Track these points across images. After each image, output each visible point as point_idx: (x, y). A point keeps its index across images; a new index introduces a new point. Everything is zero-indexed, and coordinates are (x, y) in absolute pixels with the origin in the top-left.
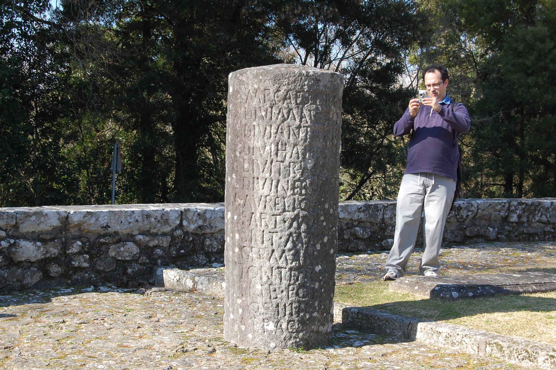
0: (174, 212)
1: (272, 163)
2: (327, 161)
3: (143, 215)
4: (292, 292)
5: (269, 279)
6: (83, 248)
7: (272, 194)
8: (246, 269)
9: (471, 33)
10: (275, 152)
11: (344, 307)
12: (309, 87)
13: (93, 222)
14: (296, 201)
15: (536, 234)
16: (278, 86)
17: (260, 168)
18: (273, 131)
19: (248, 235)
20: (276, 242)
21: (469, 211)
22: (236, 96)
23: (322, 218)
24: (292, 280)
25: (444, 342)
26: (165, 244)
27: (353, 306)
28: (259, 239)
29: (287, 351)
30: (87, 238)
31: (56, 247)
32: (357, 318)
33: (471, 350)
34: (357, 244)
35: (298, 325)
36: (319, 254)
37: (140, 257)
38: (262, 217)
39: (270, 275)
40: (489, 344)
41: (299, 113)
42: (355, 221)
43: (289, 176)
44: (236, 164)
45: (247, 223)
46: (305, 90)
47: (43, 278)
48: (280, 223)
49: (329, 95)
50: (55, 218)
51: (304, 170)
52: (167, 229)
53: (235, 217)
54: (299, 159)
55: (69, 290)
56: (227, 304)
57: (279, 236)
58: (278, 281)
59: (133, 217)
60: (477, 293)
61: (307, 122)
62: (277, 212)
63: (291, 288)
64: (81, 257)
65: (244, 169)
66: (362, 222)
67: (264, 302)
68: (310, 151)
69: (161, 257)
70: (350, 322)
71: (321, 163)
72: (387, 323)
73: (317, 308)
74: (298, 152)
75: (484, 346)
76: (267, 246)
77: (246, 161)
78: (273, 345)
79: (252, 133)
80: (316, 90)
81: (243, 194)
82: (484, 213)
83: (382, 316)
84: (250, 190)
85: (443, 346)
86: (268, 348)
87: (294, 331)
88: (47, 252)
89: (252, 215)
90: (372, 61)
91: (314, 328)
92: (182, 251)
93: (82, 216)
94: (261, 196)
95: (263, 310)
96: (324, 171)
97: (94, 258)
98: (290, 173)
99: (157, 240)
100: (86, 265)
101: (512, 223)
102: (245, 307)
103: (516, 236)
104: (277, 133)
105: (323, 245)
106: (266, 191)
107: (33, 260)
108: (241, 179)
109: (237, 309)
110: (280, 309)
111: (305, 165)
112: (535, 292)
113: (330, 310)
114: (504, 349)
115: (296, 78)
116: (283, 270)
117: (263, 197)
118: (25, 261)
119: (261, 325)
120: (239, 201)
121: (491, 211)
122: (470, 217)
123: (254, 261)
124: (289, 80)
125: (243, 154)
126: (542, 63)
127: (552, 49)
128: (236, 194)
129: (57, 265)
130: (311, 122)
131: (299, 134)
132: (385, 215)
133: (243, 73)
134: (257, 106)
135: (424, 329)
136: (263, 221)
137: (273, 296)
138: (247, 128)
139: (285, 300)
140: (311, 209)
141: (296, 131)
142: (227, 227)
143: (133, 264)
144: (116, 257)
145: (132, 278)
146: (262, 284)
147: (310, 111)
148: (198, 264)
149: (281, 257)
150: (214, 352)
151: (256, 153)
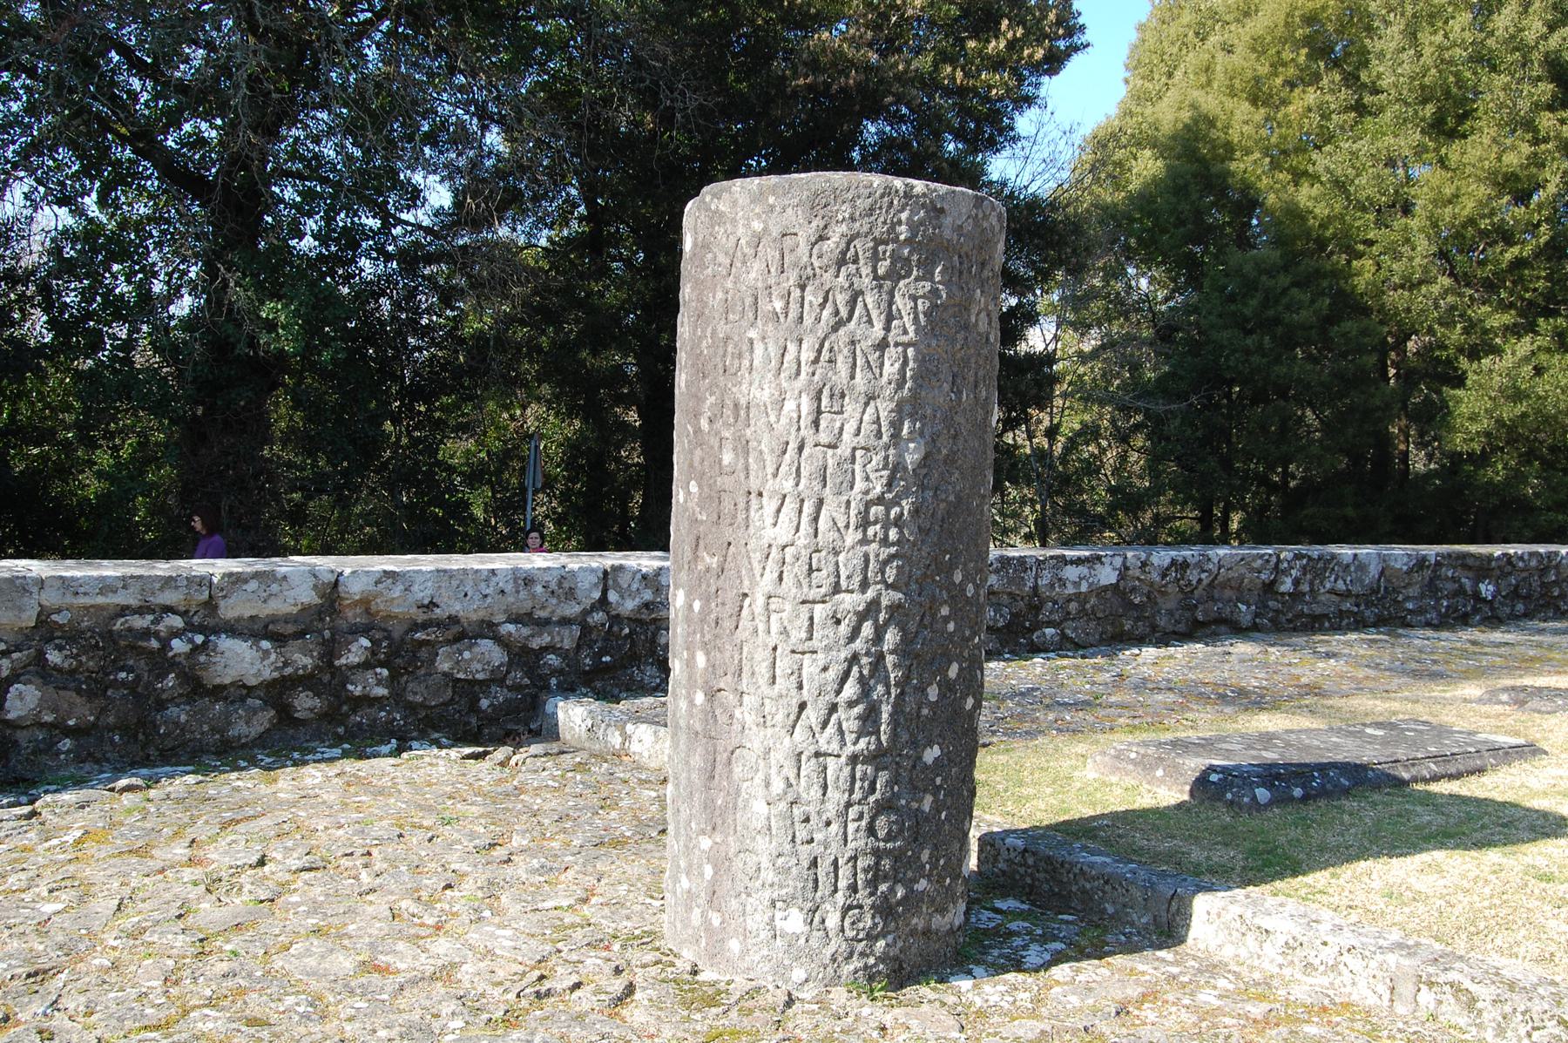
1: (801, 448)
3: (515, 580)
4: (856, 824)
5: (790, 785)
6: (374, 653)
7: (803, 539)
8: (725, 755)
9: (1148, 261)
10: (811, 418)
13: (397, 594)
14: (872, 561)
15: (1326, 616)
16: (822, 224)
17: (768, 463)
18: (807, 355)
19: (732, 657)
21: (1204, 571)
23: (945, 611)
25: (1280, 959)
26: (567, 644)
27: (1007, 827)
28: (764, 671)
29: (839, 995)
30: (385, 630)
31: (307, 652)
33: (1365, 990)
35: (873, 917)
36: (935, 713)
37: (508, 672)
38: (772, 607)
40: (1431, 984)
41: (884, 305)
43: (852, 488)
44: (698, 452)
45: (728, 624)
46: (902, 237)
47: (279, 723)
49: (967, 256)
50: (305, 586)
51: (895, 471)
52: (572, 610)
53: (697, 605)
54: (881, 438)
55: (337, 751)
57: (821, 664)
58: (815, 792)
59: (492, 584)
60: (1313, 788)
61: (905, 332)
62: (814, 594)
64: (369, 675)
67: (775, 853)
68: (913, 416)
70: (1004, 872)
71: (944, 452)
73: (928, 866)
74: (878, 418)
75: (1411, 988)
76: (784, 692)
77: (728, 446)
78: (798, 974)
79: (746, 363)
80: (931, 240)
81: (718, 538)
82: (1231, 574)
83: (1092, 865)
84: (739, 527)
85: (1278, 970)
87: (860, 936)
88: (286, 664)
89: (742, 601)
91: (918, 922)
92: (607, 659)
93: (372, 580)
94: (770, 546)
96: (951, 474)
97: (402, 675)
98: (854, 478)
100: (381, 691)
101: (1283, 594)
102: (721, 862)
103: (1290, 621)
104: (816, 361)
105: (947, 687)
106: (783, 533)
107: (253, 682)
108: (712, 497)
109: (700, 866)
111: (900, 456)
112: (1436, 778)
114: (1480, 1005)
116: (831, 762)
117: (774, 550)
118: (232, 684)
119: (766, 919)
120: (708, 559)
121: (1243, 570)
122: (1205, 582)
124: (854, 207)
125: (718, 425)
126: (1271, 313)
127: (1288, 288)
128: (698, 538)
129: (310, 694)
130: (916, 332)
131: (882, 365)
133: (722, 191)
134: (760, 284)
135: (1219, 915)
136: (774, 617)
137: (802, 835)
138: (730, 349)
139: (834, 848)
141: (873, 357)
142: (675, 630)
143: (493, 689)
145: (491, 719)
147: (914, 298)
149: (825, 724)
150: (628, 996)
151: (758, 423)
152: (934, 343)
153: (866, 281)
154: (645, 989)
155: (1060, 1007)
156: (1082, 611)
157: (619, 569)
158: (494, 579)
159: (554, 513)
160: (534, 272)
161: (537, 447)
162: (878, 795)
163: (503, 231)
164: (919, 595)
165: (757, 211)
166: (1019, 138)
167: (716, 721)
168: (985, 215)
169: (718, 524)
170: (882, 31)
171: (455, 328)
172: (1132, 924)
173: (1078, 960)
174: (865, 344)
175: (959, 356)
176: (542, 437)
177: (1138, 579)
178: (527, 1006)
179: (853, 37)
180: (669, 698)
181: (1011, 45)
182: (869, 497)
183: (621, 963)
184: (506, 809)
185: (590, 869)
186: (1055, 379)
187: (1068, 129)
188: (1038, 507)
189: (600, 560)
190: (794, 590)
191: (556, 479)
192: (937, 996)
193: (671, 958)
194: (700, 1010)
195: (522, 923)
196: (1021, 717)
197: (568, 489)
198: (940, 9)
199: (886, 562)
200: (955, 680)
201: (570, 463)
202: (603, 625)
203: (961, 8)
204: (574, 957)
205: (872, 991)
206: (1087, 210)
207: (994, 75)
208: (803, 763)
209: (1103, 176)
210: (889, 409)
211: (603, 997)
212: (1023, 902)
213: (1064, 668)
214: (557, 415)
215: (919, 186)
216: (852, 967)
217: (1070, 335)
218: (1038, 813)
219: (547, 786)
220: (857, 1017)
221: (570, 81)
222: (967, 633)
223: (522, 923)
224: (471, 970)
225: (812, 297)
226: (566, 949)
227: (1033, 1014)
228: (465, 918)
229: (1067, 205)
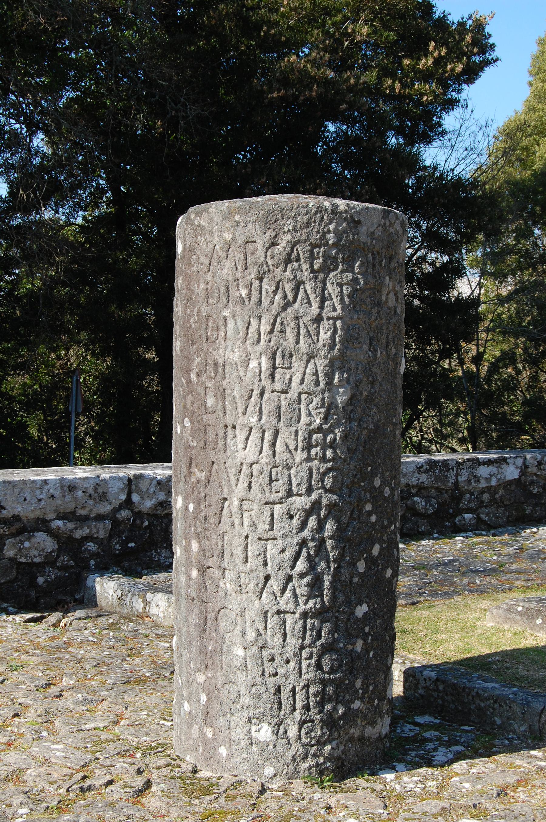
0: (116, 481)
1: (262, 394)
2: (377, 390)
3: (62, 487)
4: (308, 662)
5: (259, 635)
7: (265, 459)
8: (213, 614)
10: (268, 372)
11: (408, 665)
12: (339, 235)
14: (315, 473)
16: (273, 234)
17: (239, 405)
18: (265, 328)
19: (217, 544)
20: (273, 558)
22: (189, 260)
23: (368, 507)
24: (307, 637)
26: (102, 534)
27: (425, 663)
28: (239, 553)
29: (298, 785)
32: (435, 691)
34: (416, 523)
35: (322, 729)
36: (363, 581)
37: (58, 556)
38: (244, 507)
39: (261, 628)
41: (319, 291)
42: (413, 487)
43: (299, 421)
44: (190, 398)
45: (213, 520)
46: (331, 242)
48: (281, 520)
49: (378, 254)
52: (105, 508)
53: (191, 507)
54: (319, 385)
56: (178, 681)
57: (280, 547)
58: (278, 640)
59: (45, 490)
61: (335, 309)
62: (274, 497)
63: (305, 653)
65: (206, 409)
66: (425, 488)
67: (250, 684)
68: (341, 369)
69: (94, 555)
70: (422, 696)
71: (365, 393)
72: (496, 706)
73: (361, 691)
74: (317, 371)
76: (254, 568)
77: (211, 393)
78: (269, 771)
79: (222, 334)
80: (351, 243)
83: (485, 689)
84: (219, 451)
86: (260, 777)
87: (313, 742)
89: (223, 503)
90: (423, 259)
91: (355, 732)
92: (132, 545)
95: (248, 700)
96: (370, 409)
98: (300, 415)
99: (88, 527)
104: (271, 331)
105: (371, 561)
106: (251, 454)
109: (198, 695)
110: (283, 696)
111: (333, 397)
113: (385, 691)
115: (311, 218)
117: (245, 467)
120: (198, 474)
123: (228, 597)
124: (296, 221)
125: (203, 378)
128: (191, 459)
130: (343, 309)
132: (459, 477)
133: (202, 211)
134: (230, 278)
136: (246, 515)
137: (269, 670)
138: (210, 324)
139: (293, 679)
140: (345, 490)
141: (312, 328)
142: (176, 525)
143: (47, 569)
144: (16, 559)
146: (246, 646)
147: (340, 285)
148: (159, 565)
151: (232, 376)
152: (355, 317)
153: (306, 274)
154: (158, 783)
155: (457, 791)
156: (493, 501)
157: (139, 477)
158: (46, 487)
159: (92, 431)
160: (72, 245)
161: (78, 381)
162: (323, 640)
163: (47, 214)
164: (350, 496)
165: (227, 225)
166: (444, 133)
167: (206, 589)
168: (391, 223)
169: (205, 449)
170: (338, 53)
171: (12, 290)
172: (514, 732)
173: (472, 758)
174: (306, 319)
175: (374, 325)
176: (82, 372)
177: (536, 475)
178: (74, 797)
179: (315, 59)
180: (173, 574)
181: (438, 61)
182: (311, 428)
183: (142, 766)
184: (59, 658)
185: (120, 700)
186: (478, 318)
187: (484, 124)
188: (469, 417)
189: (125, 471)
190: (260, 495)
191: (93, 404)
192: (369, 785)
193: (178, 762)
194: (197, 798)
195: (70, 740)
196: (442, 582)
197: (103, 412)
198: (382, 35)
199: (325, 474)
200: (378, 557)
201: (103, 391)
202: (129, 519)
203: (398, 33)
204: (108, 763)
205: (322, 782)
206: (500, 187)
207: (425, 85)
208: (269, 619)
209: (513, 159)
210: (324, 364)
211: (128, 790)
212: (436, 718)
213: (478, 544)
214: (93, 354)
215: (342, 204)
216: (307, 765)
217: (489, 283)
218: (449, 653)
219: (88, 641)
220: (311, 801)
221: (97, 96)
222: (386, 523)
223: (70, 740)
224: (34, 774)
225: (268, 286)
226: (102, 757)
227: (438, 796)
228: (29, 737)
229: (485, 184)
